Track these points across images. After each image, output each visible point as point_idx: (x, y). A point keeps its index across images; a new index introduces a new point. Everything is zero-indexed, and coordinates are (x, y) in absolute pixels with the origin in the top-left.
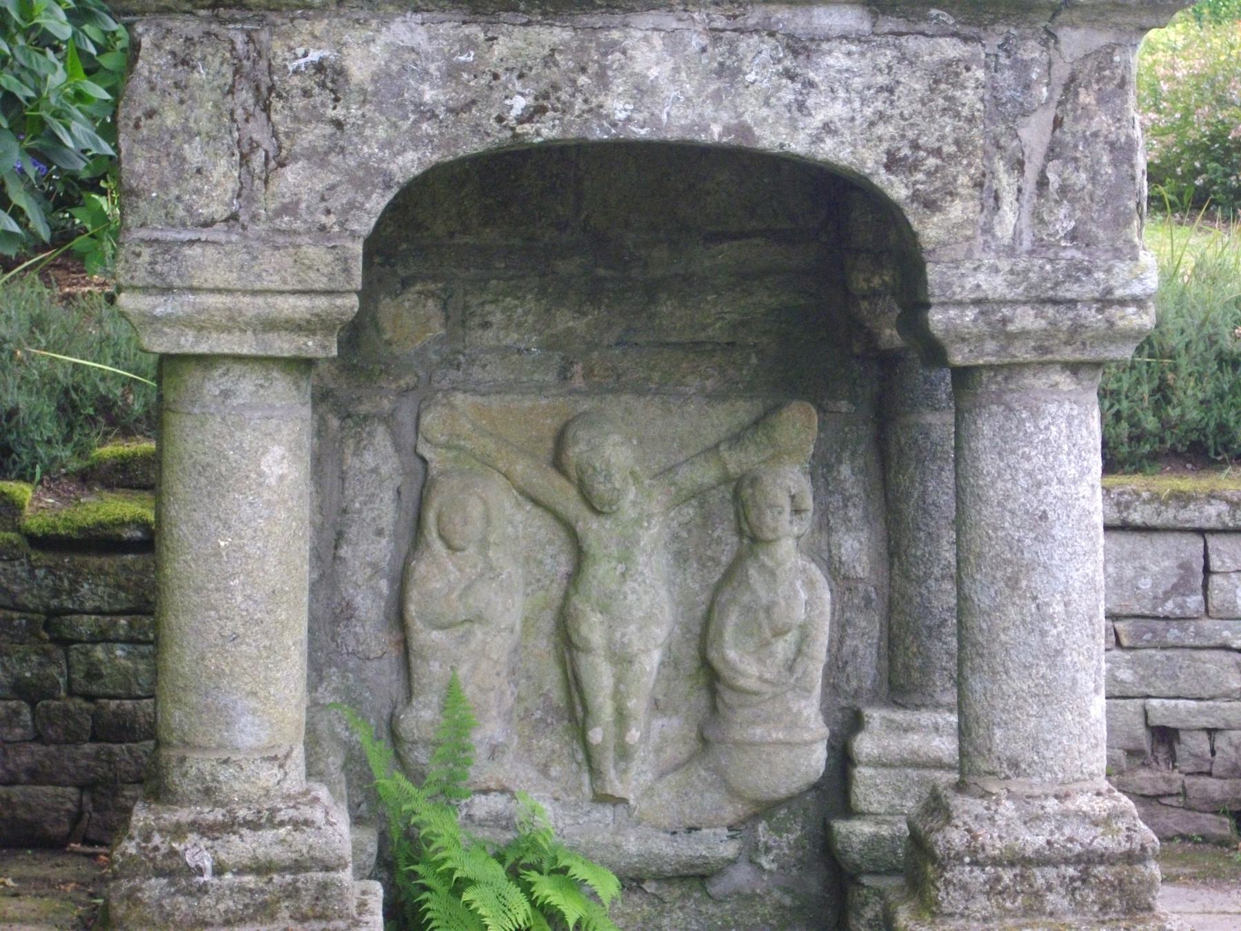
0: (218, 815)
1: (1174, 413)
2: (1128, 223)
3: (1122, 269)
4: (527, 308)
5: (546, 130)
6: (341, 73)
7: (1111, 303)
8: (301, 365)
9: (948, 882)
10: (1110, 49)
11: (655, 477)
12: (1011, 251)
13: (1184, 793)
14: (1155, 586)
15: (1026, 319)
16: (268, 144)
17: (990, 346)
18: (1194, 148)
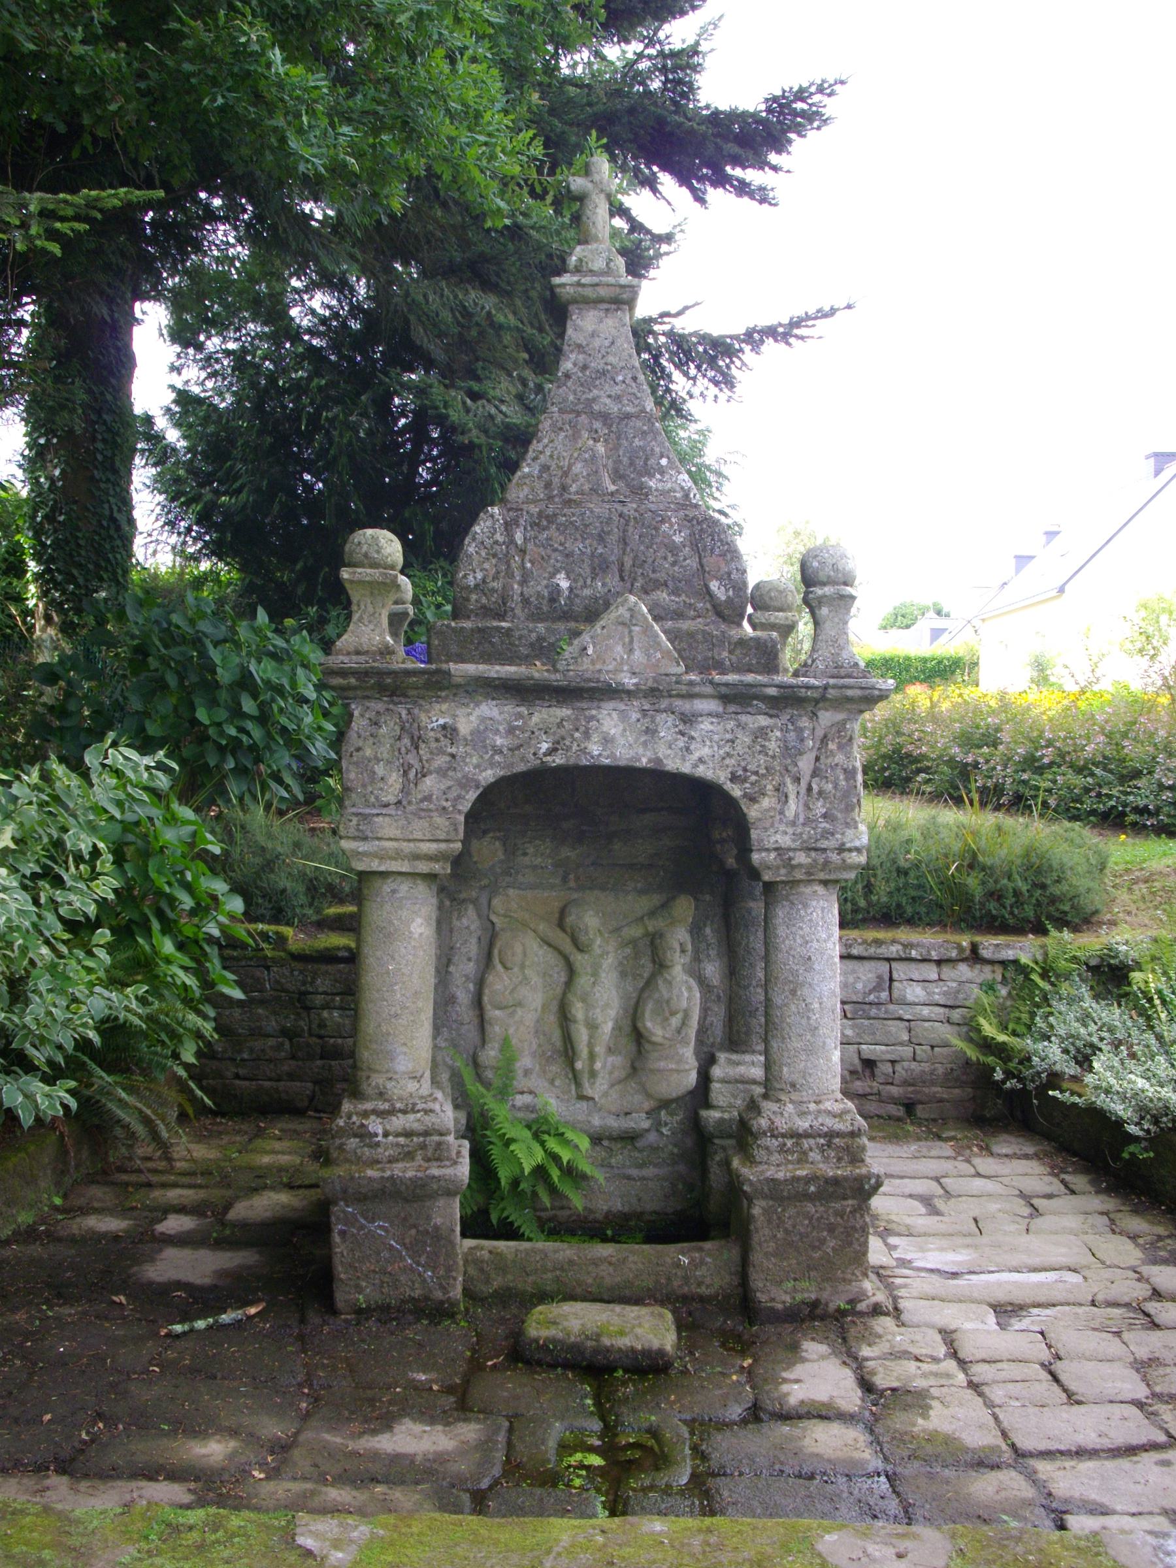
0: (386, 1106)
1: (874, 898)
3: (850, 833)
5: (558, 760)
8: (431, 877)
10: (844, 722)
12: (793, 824)
13: (879, 1093)
15: (801, 858)
16: (417, 765)
17: (783, 871)
18: (884, 757)
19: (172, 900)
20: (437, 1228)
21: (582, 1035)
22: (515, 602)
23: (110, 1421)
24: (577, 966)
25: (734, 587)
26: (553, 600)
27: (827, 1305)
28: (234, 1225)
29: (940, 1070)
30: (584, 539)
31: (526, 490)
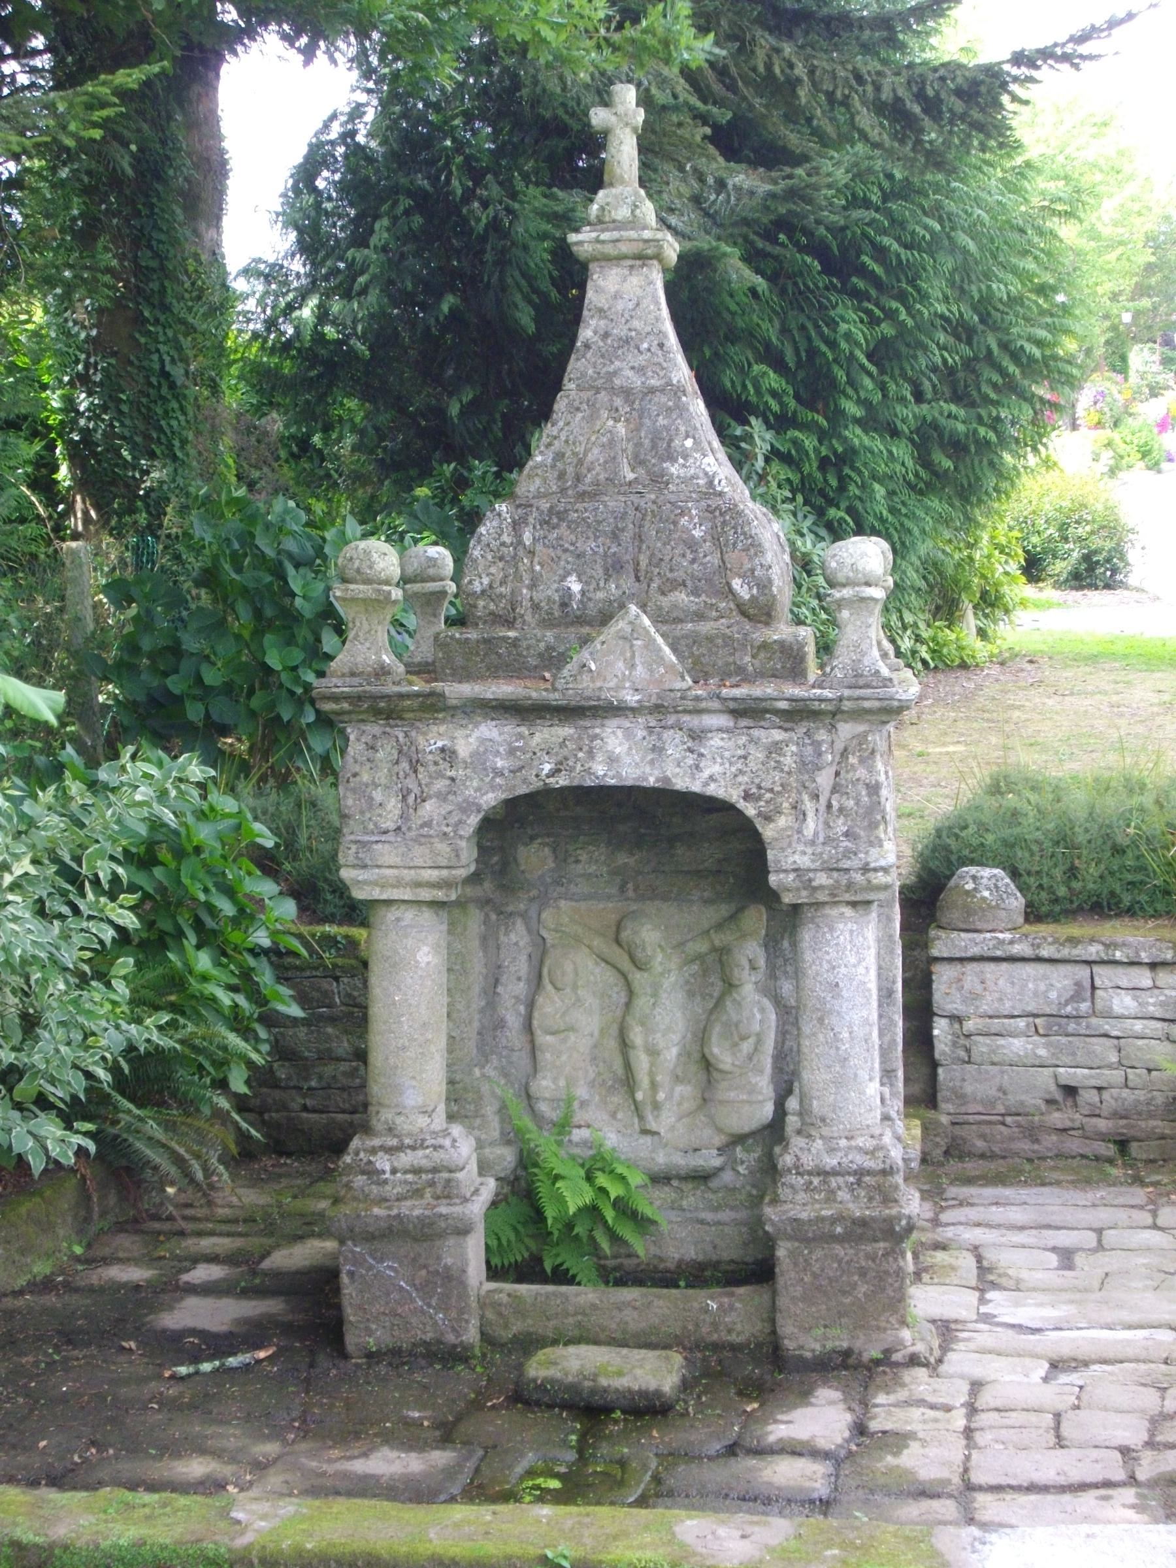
0: (394, 1142)
2: (877, 827)
3: (874, 852)
4: (601, 853)
5: (562, 781)
6: (454, 752)
7: (869, 870)
9: (783, 1184)
10: (865, 735)
11: (674, 948)
12: (813, 843)
13: (1082, 1128)
14: (1059, 996)
16: (416, 790)
17: (804, 893)
19: (211, 909)
20: (447, 1268)
21: (642, 1062)
22: (524, 609)
23: (101, 1446)
24: (636, 986)
25: (758, 585)
26: (564, 605)
27: (860, 1354)
28: (265, 1274)
29: (1160, 1099)
30: (596, 538)
31: (538, 481)
